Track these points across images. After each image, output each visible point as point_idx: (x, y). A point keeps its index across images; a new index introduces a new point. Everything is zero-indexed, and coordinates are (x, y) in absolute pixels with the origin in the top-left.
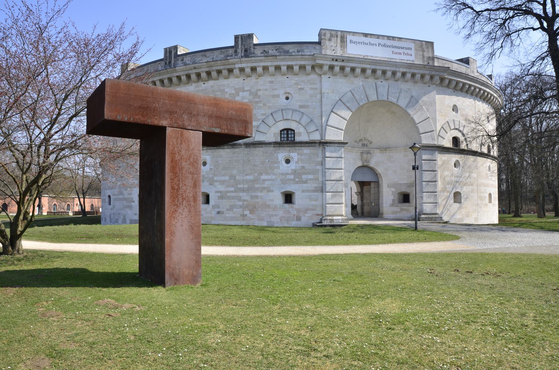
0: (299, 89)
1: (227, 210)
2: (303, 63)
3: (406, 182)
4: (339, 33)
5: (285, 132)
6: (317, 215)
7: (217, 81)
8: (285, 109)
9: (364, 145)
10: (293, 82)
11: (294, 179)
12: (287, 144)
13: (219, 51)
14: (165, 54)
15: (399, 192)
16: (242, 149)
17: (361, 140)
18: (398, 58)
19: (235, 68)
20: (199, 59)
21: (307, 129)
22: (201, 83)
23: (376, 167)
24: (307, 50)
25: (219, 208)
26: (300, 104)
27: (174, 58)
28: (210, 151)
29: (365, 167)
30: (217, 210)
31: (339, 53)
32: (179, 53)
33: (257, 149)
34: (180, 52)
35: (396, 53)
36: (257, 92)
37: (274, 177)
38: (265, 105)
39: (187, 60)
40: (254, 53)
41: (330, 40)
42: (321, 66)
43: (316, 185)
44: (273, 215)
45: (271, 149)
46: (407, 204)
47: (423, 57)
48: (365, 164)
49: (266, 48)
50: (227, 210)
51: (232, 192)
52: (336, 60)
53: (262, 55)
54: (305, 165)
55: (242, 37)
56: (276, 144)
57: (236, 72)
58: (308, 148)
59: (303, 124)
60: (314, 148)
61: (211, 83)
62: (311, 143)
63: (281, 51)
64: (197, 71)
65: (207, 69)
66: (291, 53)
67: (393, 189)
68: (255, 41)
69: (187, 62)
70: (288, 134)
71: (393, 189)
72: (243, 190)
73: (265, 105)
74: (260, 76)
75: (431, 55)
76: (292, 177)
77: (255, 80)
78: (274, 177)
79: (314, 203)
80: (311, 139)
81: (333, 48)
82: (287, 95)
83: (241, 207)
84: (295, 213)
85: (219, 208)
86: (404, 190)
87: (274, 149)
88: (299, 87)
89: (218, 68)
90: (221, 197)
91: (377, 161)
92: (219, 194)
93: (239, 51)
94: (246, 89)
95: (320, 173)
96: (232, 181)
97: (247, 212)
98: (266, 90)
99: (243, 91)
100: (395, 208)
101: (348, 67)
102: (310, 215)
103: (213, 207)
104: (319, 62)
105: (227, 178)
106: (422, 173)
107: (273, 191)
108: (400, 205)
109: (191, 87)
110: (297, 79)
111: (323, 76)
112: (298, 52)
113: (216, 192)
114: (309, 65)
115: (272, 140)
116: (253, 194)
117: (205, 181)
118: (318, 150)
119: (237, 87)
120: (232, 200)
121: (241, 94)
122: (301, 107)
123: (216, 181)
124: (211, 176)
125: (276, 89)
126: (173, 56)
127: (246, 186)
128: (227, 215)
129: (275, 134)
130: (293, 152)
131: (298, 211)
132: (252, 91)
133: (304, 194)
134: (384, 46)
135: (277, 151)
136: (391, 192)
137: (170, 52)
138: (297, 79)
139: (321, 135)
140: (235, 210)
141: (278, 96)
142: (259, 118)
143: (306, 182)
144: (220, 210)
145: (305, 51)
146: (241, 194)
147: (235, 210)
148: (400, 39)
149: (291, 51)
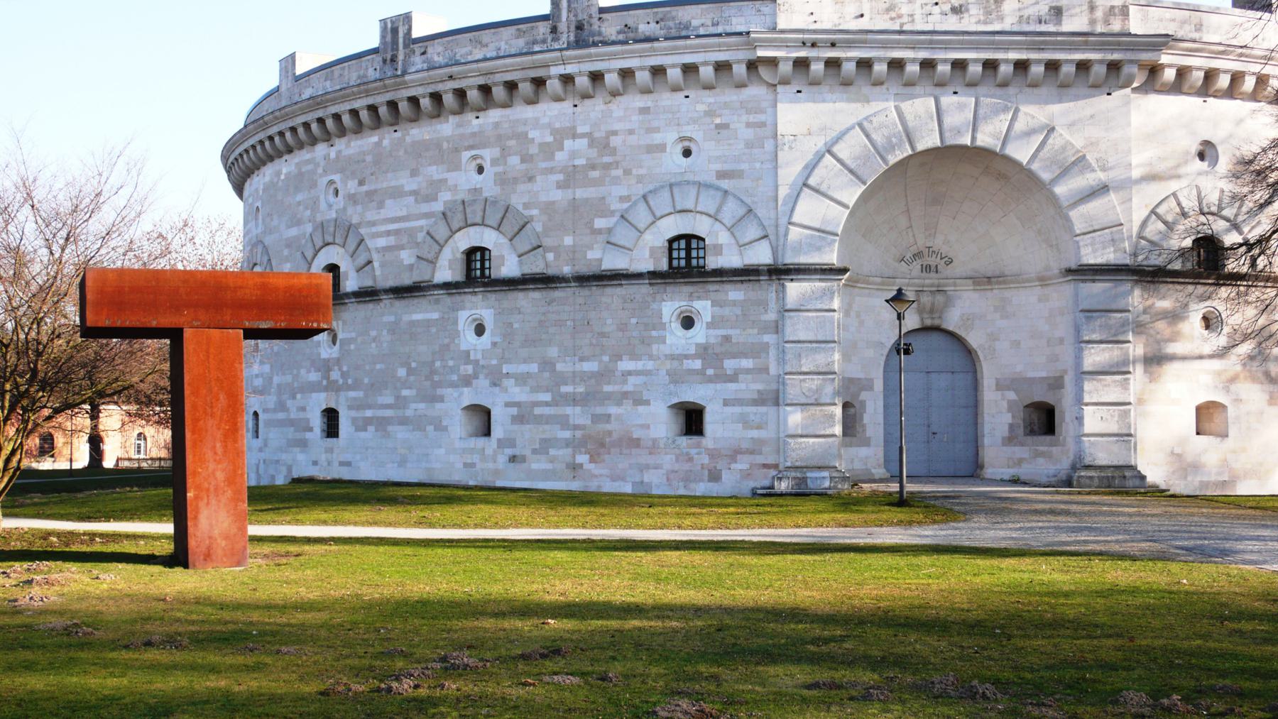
0: (718, 127)
1: (534, 451)
3: (1044, 374)
5: (683, 244)
6: (765, 466)
7: (508, 111)
8: (679, 184)
9: (927, 269)
10: (701, 108)
13: (511, 30)
17: (918, 255)
19: (550, 77)
20: (464, 51)
21: (737, 234)
22: (470, 116)
23: (961, 332)
26: (718, 166)
27: (406, 46)
28: (492, 297)
30: (509, 452)
32: (416, 34)
33: (609, 290)
36: (607, 138)
37: (650, 365)
38: (627, 172)
42: (773, 62)
44: (647, 467)
45: (642, 290)
46: (1048, 438)
48: (928, 322)
50: (534, 451)
51: (547, 404)
54: (730, 332)
57: (554, 85)
58: (739, 285)
59: (726, 221)
60: (757, 285)
61: (494, 115)
62: (747, 274)
63: (671, 24)
65: (481, 81)
66: (697, 28)
67: (1012, 395)
69: (436, 58)
70: (688, 249)
71: (1012, 395)
72: (574, 400)
73: (627, 172)
74: (615, 94)
76: (697, 364)
77: (603, 107)
78: (650, 365)
79: (755, 434)
82: (686, 144)
83: (567, 446)
84: (706, 460)
86: (1040, 395)
88: (718, 121)
89: (509, 77)
90: (519, 419)
92: (514, 411)
93: (562, 26)
94: (580, 130)
95: (772, 353)
96: (547, 375)
97: (582, 459)
98: (631, 132)
100: (1016, 449)
103: (501, 444)
105: (534, 368)
106: (1081, 350)
107: (647, 403)
108: (1029, 439)
109: (445, 126)
110: (711, 100)
111: (780, 88)
113: (508, 405)
114: (739, 62)
115: (646, 265)
116: (599, 410)
117: (481, 376)
119: (557, 125)
120: (547, 427)
121: (568, 144)
122: (722, 175)
124: (494, 362)
125: (657, 130)
126: (401, 41)
127: (581, 389)
128: (534, 466)
129: (652, 250)
130: (699, 298)
131: (714, 454)
132: (597, 135)
133: (729, 410)
135: (658, 296)
136: (1005, 404)
138: (711, 100)
140: (552, 452)
142: (613, 208)
143: (733, 378)
144: (517, 451)
145: (734, 20)
146: (569, 410)
147: (552, 452)
149: (695, 23)
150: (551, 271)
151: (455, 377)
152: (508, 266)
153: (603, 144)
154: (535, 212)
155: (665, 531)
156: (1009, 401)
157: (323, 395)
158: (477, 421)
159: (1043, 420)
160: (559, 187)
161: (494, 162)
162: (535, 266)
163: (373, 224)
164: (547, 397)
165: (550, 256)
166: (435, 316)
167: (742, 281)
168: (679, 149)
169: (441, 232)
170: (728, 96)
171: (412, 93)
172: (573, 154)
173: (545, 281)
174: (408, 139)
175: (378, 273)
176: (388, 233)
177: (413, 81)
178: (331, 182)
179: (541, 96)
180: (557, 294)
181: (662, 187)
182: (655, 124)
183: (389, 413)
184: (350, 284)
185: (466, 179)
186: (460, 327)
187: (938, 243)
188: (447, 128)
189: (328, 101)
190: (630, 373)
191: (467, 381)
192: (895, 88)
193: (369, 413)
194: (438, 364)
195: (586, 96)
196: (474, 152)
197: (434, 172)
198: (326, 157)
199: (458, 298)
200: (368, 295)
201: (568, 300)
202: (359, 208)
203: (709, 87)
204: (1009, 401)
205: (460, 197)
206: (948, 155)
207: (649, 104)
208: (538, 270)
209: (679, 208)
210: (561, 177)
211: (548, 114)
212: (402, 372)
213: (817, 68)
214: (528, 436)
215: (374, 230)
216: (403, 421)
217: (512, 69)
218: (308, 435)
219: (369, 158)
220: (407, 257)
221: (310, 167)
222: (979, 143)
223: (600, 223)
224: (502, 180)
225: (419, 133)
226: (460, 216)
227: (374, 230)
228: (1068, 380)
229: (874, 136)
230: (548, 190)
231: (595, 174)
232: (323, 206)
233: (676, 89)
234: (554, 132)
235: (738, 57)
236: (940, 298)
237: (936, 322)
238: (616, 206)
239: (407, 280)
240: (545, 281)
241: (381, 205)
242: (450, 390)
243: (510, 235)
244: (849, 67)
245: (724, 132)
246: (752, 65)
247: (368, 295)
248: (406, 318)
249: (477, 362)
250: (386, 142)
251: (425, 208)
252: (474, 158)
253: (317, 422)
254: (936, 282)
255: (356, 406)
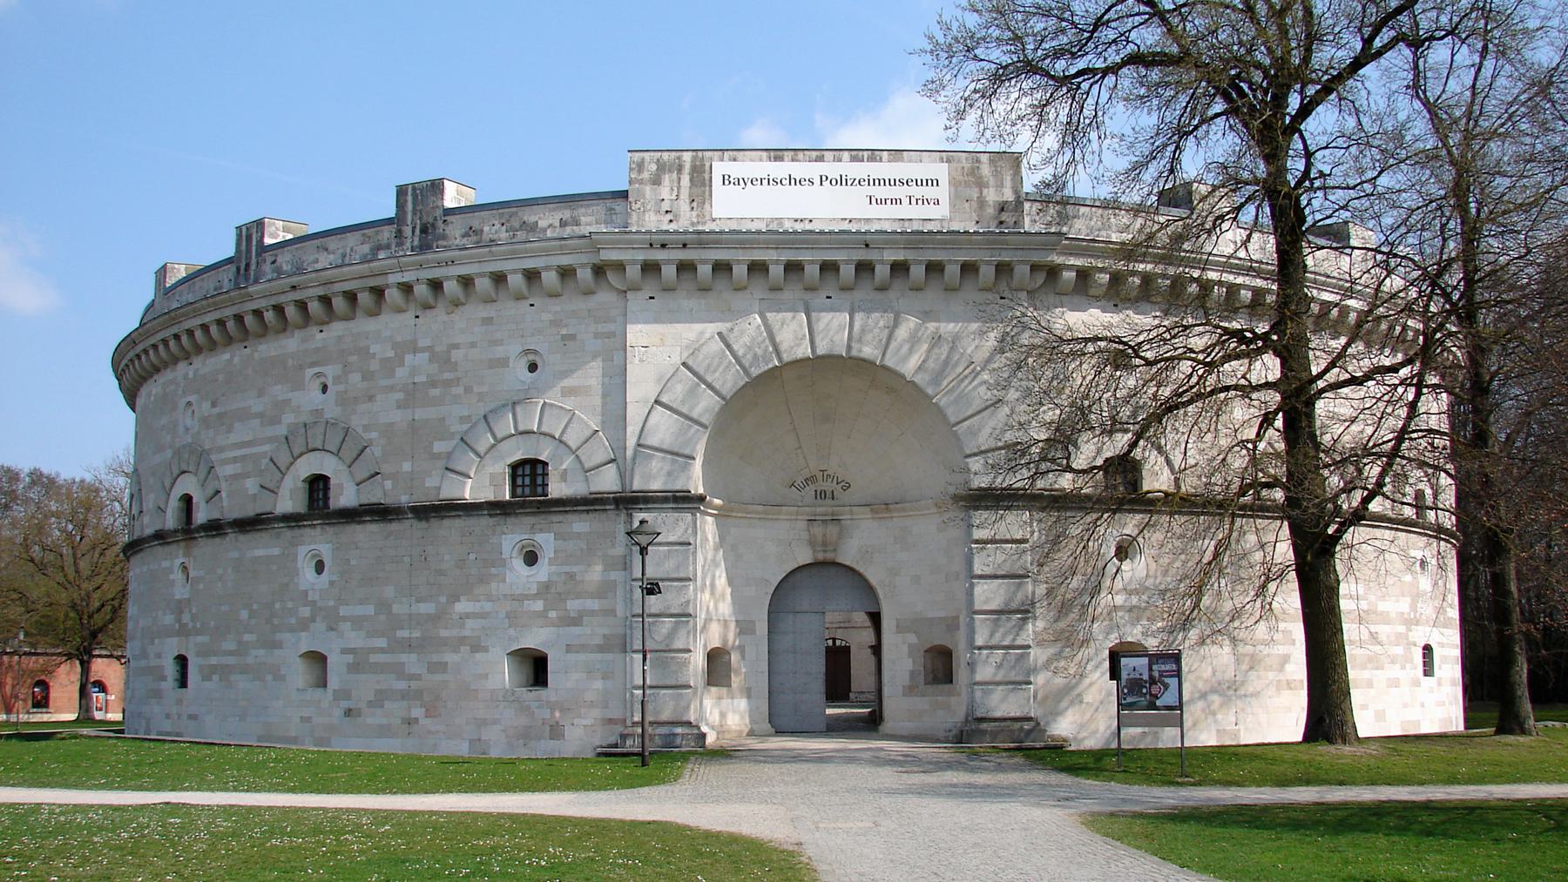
0: (564, 337)
1: (370, 704)
2: (565, 261)
3: (942, 614)
4: (687, 157)
6: (610, 721)
7: (351, 324)
9: (821, 495)
10: (546, 317)
11: (546, 610)
12: (523, 505)
14: (400, 205)
15: (928, 646)
16: (407, 523)
17: (811, 479)
18: (885, 217)
20: (312, 258)
21: (583, 458)
22: (314, 330)
24: (589, 219)
25: (349, 698)
27: (259, 254)
28: (330, 530)
29: (826, 570)
30: (345, 704)
31: (686, 220)
32: (268, 241)
33: (447, 522)
34: (273, 236)
35: (880, 202)
36: (448, 351)
37: (488, 606)
38: (468, 390)
39: (285, 260)
40: (444, 237)
41: (656, 181)
42: (620, 267)
43: (606, 631)
45: (483, 522)
46: (947, 687)
47: (982, 203)
48: (821, 556)
49: (475, 220)
51: (382, 650)
52: (663, 246)
53: (465, 241)
54: (575, 569)
55: (414, 189)
56: (497, 509)
57: (393, 295)
58: (584, 516)
59: (570, 443)
60: (604, 515)
61: (337, 328)
62: (591, 503)
64: (297, 295)
65: (321, 291)
66: (545, 230)
67: (912, 638)
68: (450, 201)
70: (534, 476)
71: (912, 638)
72: (409, 646)
73: (468, 390)
74: (457, 304)
75: (1009, 196)
77: (446, 318)
78: (488, 606)
80: (593, 489)
81: (666, 206)
82: (531, 357)
83: (403, 698)
85: (349, 698)
86: (939, 639)
87: (491, 521)
88: (564, 332)
90: (355, 668)
91: (860, 544)
92: (350, 658)
93: (407, 231)
94: (421, 344)
95: (620, 593)
96: (382, 617)
97: (417, 712)
98: (473, 345)
99: (415, 351)
101: (704, 262)
102: (588, 722)
104: (614, 256)
106: (972, 586)
107: (486, 650)
108: (930, 689)
110: (558, 308)
112: (563, 224)
113: (344, 651)
114: (583, 266)
115: (488, 495)
116: (435, 658)
117: (318, 619)
118: (616, 524)
119: (399, 339)
121: (408, 358)
123: (345, 619)
124: (331, 603)
125: (499, 343)
127: (416, 634)
128: (369, 721)
130: (541, 531)
133: (572, 657)
134: (841, 181)
135: (498, 529)
136: (905, 649)
137: (249, 237)
138: (558, 308)
139: (622, 476)
140: (388, 704)
141: (503, 362)
142: (453, 429)
143: (576, 621)
146: (404, 658)
147: (388, 704)
148: (897, 154)
149: (542, 224)
150: (389, 501)
151: (293, 621)
152: (345, 495)
153: (443, 359)
154: (374, 435)
155: (116, 802)
156: (910, 645)
157: (175, 640)
158: (528, 670)
159: (940, 666)
160: (399, 407)
161: (337, 380)
162: (373, 495)
163: (221, 450)
164: (382, 643)
165: (388, 484)
166: (276, 551)
167: (588, 511)
168: (523, 365)
169: (283, 458)
170: (572, 304)
171: (255, 305)
172: (414, 371)
173: (382, 513)
174: (256, 355)
175: (225, 504)
176: (235, 460)
177: (257, 292)
178: (189, 404)
179: (384, 307)
180: (394, 526)
181: (504, 406)
182: (498, 336)
183: (231, 660)
184: (201, 516)
185: (311, 398)
186: (299, 564)
187: (833, 466)
188: (291, 343)
189: (183, 315)
190: (465, 617)
191: (304, 625)
192: (758, 291)
193: (214, 660)
194: (277, 606)
195: (427, 307)
196: (317, 370)
197: (279, 391)
198: (186, 376)
199: (297, 532)
200: (215, 528)
201: (409, 528)
202: (211, 433)
203: (554, 295)
204: (910, 645)
205: (303, 418)
206: (821, 366)
207: (493, 314)
208: (374, 500)
209: (521, 428)
210: (400, 395)
211: (392, 325)
212: (244, 614)
213: (669, 272)
214: (366, 686)
215: (223, 456)
216: (245, 670)
217: (352, 277)
218: (164, 685)
219: (221, 377)
220: (251, 485)
221: (172, 387)
222: (820, 352)
223: (440, 447)
224: (342, 400)
225: (268, 349)
226: (301, 440)
227: (223, 456)
228: (963, 620)
229: (735, 347)
230: (387, 411)
231: (435, 392)
232: (181, 429)
233: (519, 297)
234: (395, 345)
235: (581, 261)
236: (832, 530)
237: (830, 556)
238: (458, 428)
239: (250, 511)
240: (382, 513)
241: (230, 430)
242: (288, 635)
243: (348, 461)
244: (705, 270)
245: (570, 344)
246: (599, 270)
247: (215, 528)
248: (249, 554)
249: (314, 602)
250: (236, 360)
251: (270, 431)
252: (318, 375)
253: (171, 670)
254: (830, 510)
255: (204, 652)
